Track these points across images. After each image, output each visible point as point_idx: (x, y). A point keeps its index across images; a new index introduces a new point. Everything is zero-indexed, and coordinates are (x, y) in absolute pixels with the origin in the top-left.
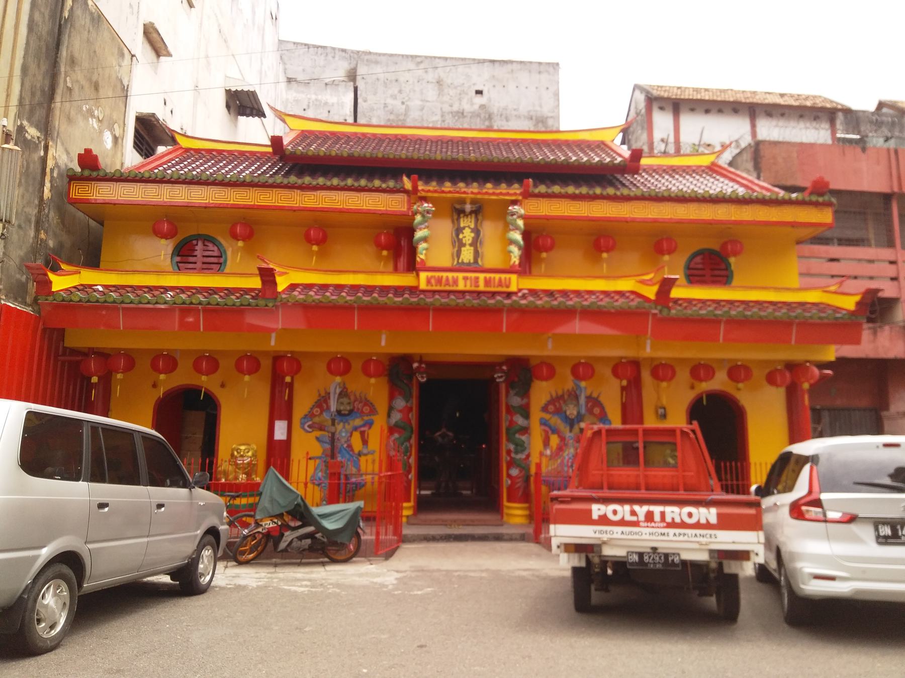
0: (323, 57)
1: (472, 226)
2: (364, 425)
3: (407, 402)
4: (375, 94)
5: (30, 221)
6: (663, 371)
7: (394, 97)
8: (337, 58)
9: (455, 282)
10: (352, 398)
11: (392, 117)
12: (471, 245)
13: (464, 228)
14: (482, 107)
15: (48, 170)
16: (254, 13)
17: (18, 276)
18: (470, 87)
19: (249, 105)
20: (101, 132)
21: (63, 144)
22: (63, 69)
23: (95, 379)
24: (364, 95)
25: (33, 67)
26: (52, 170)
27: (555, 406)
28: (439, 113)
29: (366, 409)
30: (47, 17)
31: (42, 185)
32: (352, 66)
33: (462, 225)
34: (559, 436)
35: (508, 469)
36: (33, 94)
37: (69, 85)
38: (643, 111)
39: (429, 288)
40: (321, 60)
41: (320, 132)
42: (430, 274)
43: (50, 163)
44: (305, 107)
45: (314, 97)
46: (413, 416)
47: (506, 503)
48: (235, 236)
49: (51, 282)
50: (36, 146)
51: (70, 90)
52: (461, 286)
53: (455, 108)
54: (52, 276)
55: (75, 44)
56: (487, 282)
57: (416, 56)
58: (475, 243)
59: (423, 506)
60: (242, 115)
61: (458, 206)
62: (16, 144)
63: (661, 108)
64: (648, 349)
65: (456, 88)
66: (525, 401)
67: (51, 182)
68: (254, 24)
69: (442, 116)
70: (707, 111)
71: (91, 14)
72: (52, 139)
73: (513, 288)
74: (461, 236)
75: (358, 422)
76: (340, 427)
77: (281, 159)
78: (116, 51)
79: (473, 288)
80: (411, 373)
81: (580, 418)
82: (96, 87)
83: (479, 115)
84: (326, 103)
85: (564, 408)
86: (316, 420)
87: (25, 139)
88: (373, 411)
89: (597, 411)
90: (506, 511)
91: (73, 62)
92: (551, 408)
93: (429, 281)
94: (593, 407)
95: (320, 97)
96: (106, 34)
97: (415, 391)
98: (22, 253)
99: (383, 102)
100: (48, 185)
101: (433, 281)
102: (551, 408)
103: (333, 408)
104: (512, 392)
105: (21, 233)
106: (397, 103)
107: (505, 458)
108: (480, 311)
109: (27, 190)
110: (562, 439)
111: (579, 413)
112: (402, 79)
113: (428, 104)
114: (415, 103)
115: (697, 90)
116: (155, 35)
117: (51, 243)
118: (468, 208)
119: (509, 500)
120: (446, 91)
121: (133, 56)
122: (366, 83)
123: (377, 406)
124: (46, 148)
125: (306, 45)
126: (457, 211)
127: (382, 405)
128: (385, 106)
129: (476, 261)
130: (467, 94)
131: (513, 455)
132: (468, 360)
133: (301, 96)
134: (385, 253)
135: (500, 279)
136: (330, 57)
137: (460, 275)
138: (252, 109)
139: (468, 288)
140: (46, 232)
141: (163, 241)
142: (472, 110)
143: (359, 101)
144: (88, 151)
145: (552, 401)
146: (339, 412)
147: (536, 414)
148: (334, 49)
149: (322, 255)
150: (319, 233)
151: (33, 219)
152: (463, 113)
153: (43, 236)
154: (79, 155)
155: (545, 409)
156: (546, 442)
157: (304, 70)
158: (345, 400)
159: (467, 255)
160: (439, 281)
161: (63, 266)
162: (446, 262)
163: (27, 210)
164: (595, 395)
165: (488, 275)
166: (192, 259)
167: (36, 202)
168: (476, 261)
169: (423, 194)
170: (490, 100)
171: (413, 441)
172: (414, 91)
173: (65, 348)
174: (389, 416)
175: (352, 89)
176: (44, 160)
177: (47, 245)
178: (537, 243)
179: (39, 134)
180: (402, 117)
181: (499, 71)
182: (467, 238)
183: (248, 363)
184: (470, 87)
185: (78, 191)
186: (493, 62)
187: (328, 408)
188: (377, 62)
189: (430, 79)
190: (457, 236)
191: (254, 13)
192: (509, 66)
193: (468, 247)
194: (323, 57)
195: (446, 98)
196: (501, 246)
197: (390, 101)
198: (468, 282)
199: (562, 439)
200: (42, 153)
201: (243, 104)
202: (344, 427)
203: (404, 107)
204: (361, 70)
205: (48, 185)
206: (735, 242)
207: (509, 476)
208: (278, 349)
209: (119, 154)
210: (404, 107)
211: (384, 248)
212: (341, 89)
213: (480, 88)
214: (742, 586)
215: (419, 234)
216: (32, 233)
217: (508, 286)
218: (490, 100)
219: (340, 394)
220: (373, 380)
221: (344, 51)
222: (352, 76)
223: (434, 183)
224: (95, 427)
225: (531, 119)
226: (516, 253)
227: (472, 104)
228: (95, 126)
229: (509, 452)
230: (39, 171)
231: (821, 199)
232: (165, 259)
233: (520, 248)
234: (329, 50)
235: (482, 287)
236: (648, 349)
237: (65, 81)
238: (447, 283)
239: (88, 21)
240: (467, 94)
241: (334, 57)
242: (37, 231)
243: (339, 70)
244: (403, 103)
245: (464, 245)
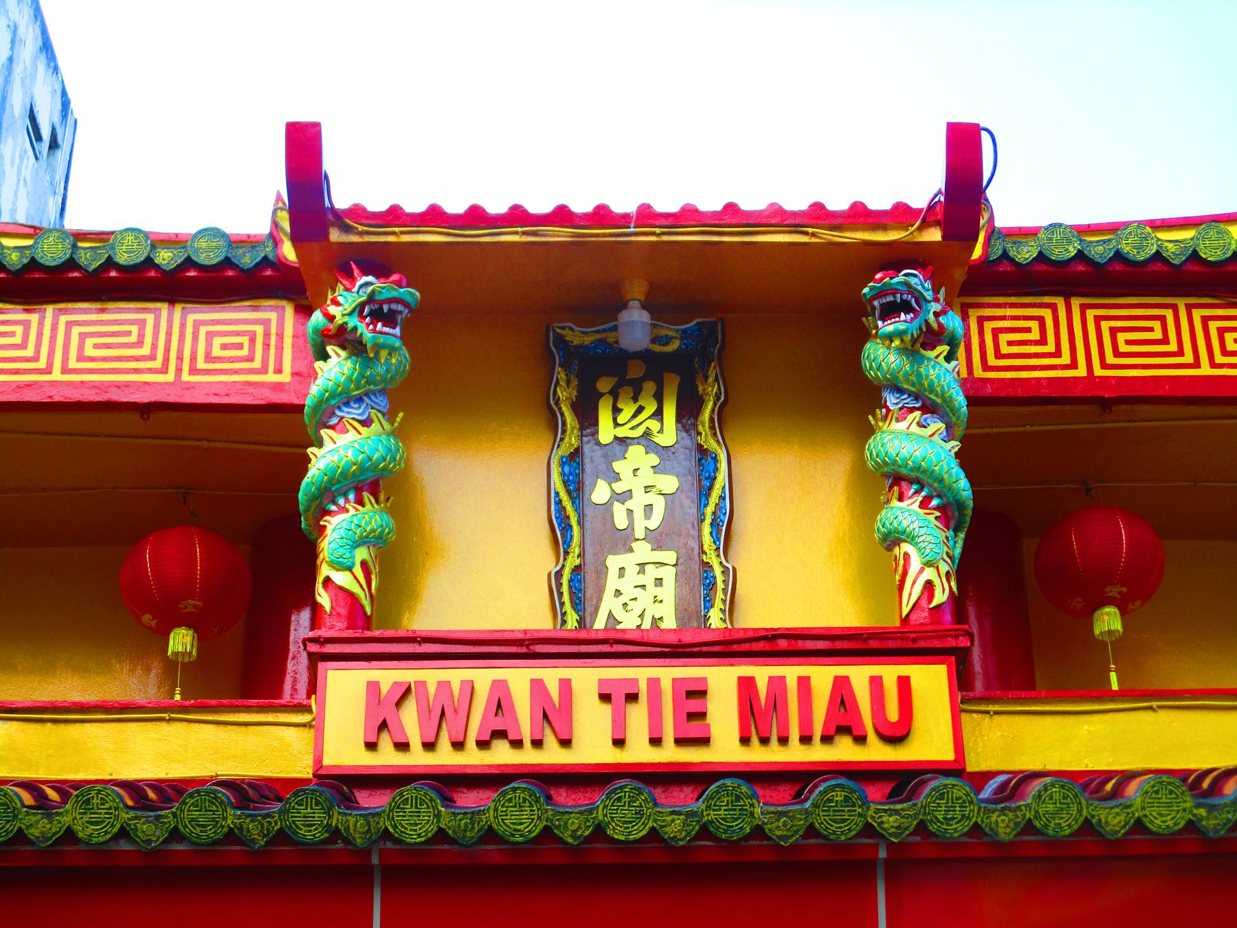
9: (555, 717)
12: (658, 539)
39: (387, 758)
42: (389, 677)
52: (592, 746)
61: (577, 336)
74: (600, 493)
79: (670, 754)
93: (380, 727)
101: (410, 720)
135: (444, 686)
137: (585, 679)
139: (639, 752)
159: (640, 593)
160: (443, 716)
162: (531, 614)
182: (638, 503)
190: (577, 488)
193: (643, 551)
198: (638, 716)
214: (878, 862)
217: (896, 735)
226: (928, 560)
233: (949, 515)
235: (726, 747)
245: (623, 540)
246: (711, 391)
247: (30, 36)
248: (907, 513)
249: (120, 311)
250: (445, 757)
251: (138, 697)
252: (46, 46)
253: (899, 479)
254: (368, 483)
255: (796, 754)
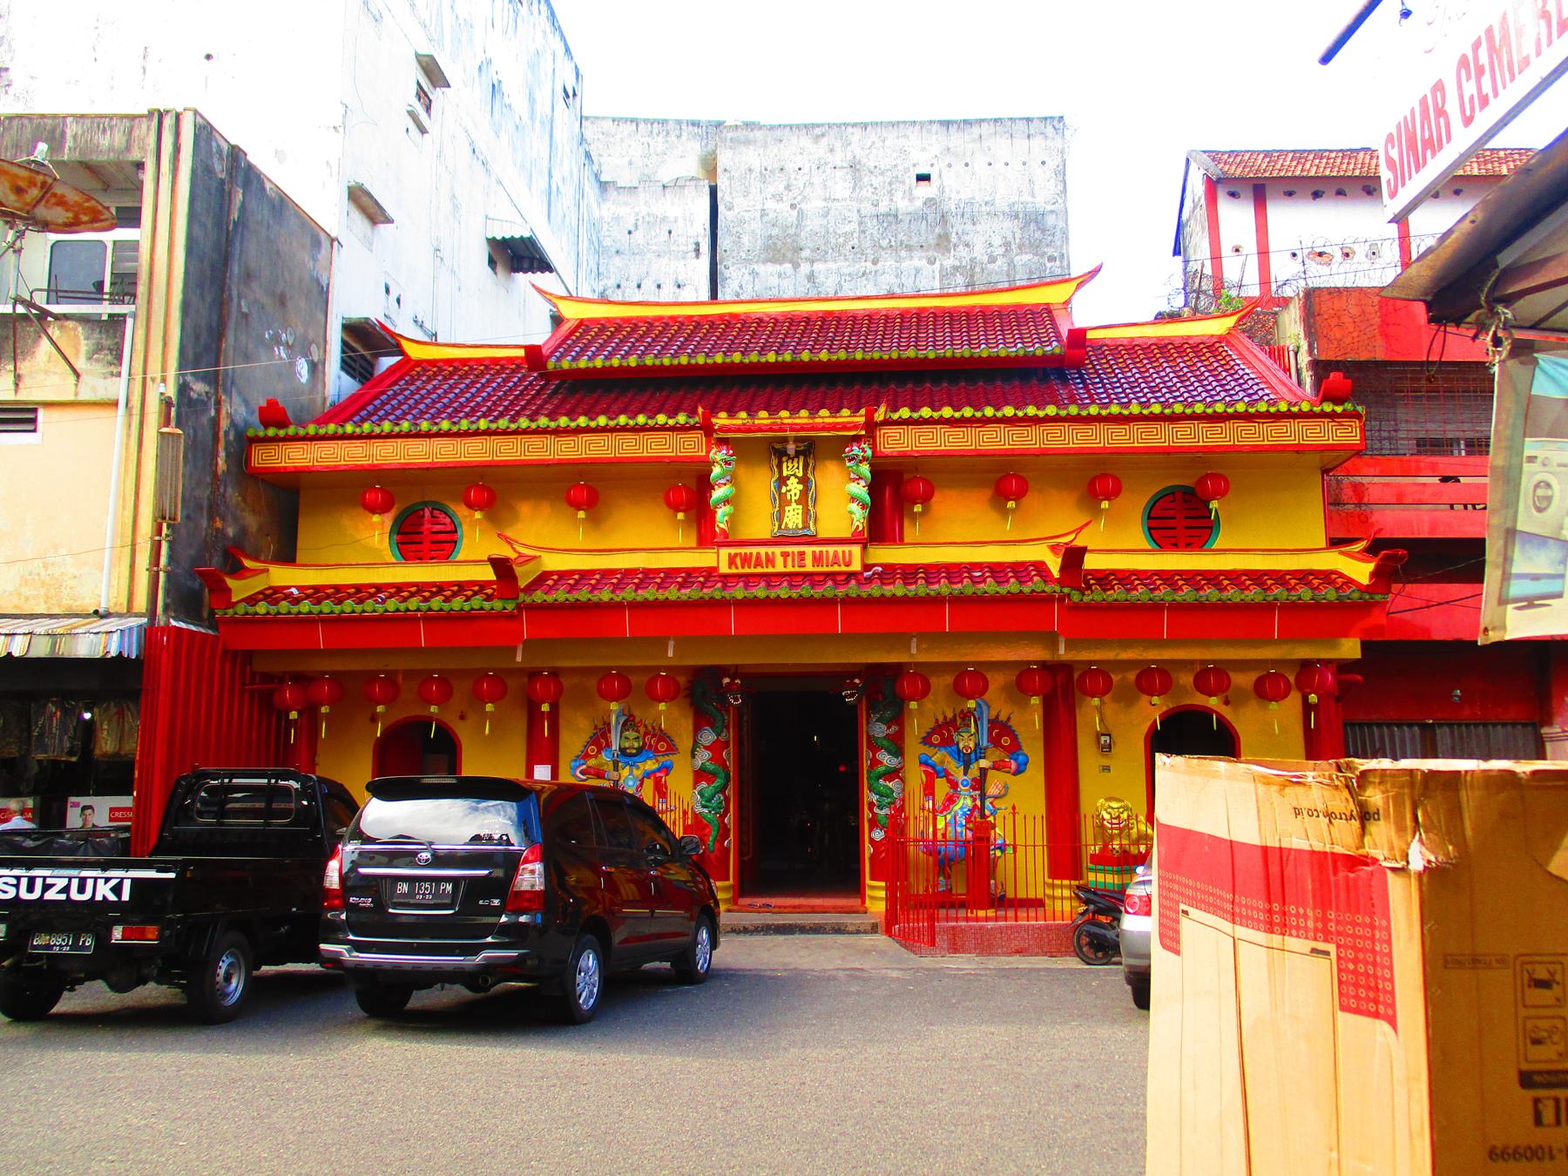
0: (661, 139)
1: (800, 474)
2: (659, 770)
3: (718, 735)
4: (746, 194)
5: (201, 508)
6: (1097, 680)
7: (779, 198)
8: (684, 138)
9: (770, 560)
10: (642, 729)
11: (775, 232)
12: (798, 502)
13: (788, 478)
14: (930, 202)
15: (222, 434)
16: (532, 100)
17: (189, 583)
18: (907, 170)
19: (526, 254)
20: (292, 365)
21: (240, 393)
22: (235, 293)
23: (294, 715)
24: (728, 198)
25: (195, 300)
26: (227, 433)
27: (942, 735)
28: (855, 218)
29: (662, 746)
30: (210, 226)
31: (215, 455)
32: (710, 148)
33: (785, 473)
34: (949, 781)
35: (871, 830)
36: (197, 338)
37: (245, 310)
38: (1203, 201)
39: (734, 571)
40: (658, 143)
41: (609, 320)
42: (733, 551)
43: (224, 424)
44: (631, 228)
45: (644, 211)
46: (728, 755)
47: (868, 881)
48: (471, 506)
49: (229, 590)
50: (205, 404)
51: (246, 316)
53: (883, 209)
54: (231, 582)
55: (251, 252)
56: (817, 559)
57: (814, 126)
58: (803, 499)
59: (745, 888)
60: (517, 270)
61: (778, 446)
62: (177, 426)
63: (1233, 195)
64: (1062, 651)
65: (882, 174)
66: (894, 729)
67: (226, 449)
68: (532, 119)
69: (860, 224)
70: (1316, 195)
71: (271, 200)
72: (225, 391)
73: (856, 566)
74: (784, 490)
75: (651, 765)
76: (625, 772)
77: (541, 376)
78: (308, 241)
79: (797, 569)
80: (722, 692)
81: (979, 753)
82: (282, 301)
83: (924, 218)
84: (664, 219)
85: (956, 738)
86: (592, 762)
87: (190, 399)
88: (672, 749)
89: (1006, 741)
90: (868, 892)
91: (248, 276)
92: (936, 739)
93: (732, 561)
94: (1000, 736)
95: (654, 210)
96: (293, 223)
97: (730, 718)
98: (192, 552)
99: (759, 207)
100: (222, 454)
101: (738, 561)
102: (936, 739)
103: (615, 747)
104: (874, 717)
105: (191, 524)
106: (784, 207)
107: (867, 814)
108: (809, 605)
109: (195, 467)
110: (954, 785)
111: (977, 745)
112: (791, 167)
113: (836, 204)
114: (814, 205)
115: (1300, 155)
116: (365, 200)
117: (230, 532)
118: (791, 448)
119: (872, 878)
120: (866, 180)
121: (333, 240)
122: (730, 179)
123: (677, 741)
124: (218, 403)
125: (632, 121)
126: (775, 450)
127: (684, 741)
128: (764, 213)
129: (806, 526)
130: (903, 182)
131: (876, 810)
132: (786, 670)
133: (623, 211)
134: (681, 516)
136: (673, 138)
137: (778, 550)
138: (532, 259)
139: (790, 569)
140: (223, 519)
141: (376, 518)
142: (911, 209)
143: (721, 208)
144: (272, 404)
145: (938, 729)
146: (623, 751)
147: (914, 748)
148: (679, 122)
149: (595, 521)
150: (585, 491)
151: (205, 503)
152: (896, 216)
153: (219, 524)
154: (261, 409)
155: (926, 740)
156: (929, 790)
157: (630, 163)
158: (631, 734)
159: (793, 517)
160: (746, 560)
161: (248, 563)
163: (197, 493)
164: (1003, 718)
165: (817, 549)
166: (417, 538)
167: (208, 480)
168: (806, 526)
169: (722, 435)
170: (942, 189)
171: (730, 792)
172: (812, 184)
173: (253, 674)
174: (693, 756)
175: (707, 191)
176: (216, 423)
177: (225, 535)
178: (895, 495)
179: (207, 389)
180: (792, 231)
181: (956, 139)
183: (491, 686)
184: (907, 170)
185: (264, 458)
186: (946, 124)
187: (609, 745)
188: (747, 142)
189: (839, 164)
190: (780, 488)
191: (532, 100)
192: (976, 130)
193: (794, 505)
194: (661, 139)
195: (867, 193)
196: (842, 500)
197: (771, 205)
198: (789, 560)
199: (954, 785)
200: (213, 413)
201: (518, 256)
202: (631, 773)
203: (795, 213)
204: (724, 159)
205: (222, 454)
206: (1217, 478)
207: (872, 841)
208: (527, 665)
209: (320, 387)
210: (795, 213)
211: (677, 510)
212: (690, 191)
213: (925, 171)
215: (718, 494)
216: (204, 523)
217: (848, 565)
218: (942, 189)
219: (624, 724)
220: (662, 706)
221: (695, 124)
222: (710, 167)
223: (743, 415)
224: (1159, 643)
225: (1017, 217)
226: (859, 516)
227: (911, 200)
228: (284, 355)
229: (871, 805)
230: (210, 437)
231: (1339, 409)
232: (381, 541)
234: (671, 125)
235: (809, 567)
236: (1062, 651)
237: (239, 305)
238: (758, 563)
239: (266, 212)
240: (903, 182)
241: (679, 136)
242: (211, 518)
243: (685, 160)
244: (793, 206)
245: (789, 503)
246: (811, 462)
247: (561, 50)
248: (854, 507)
249: (781, 909)
250: (747, 570)
251: (538, 107)
252: (567, 50)
253: (853, 499)
254: (727, 501)
255: (825, 569)
